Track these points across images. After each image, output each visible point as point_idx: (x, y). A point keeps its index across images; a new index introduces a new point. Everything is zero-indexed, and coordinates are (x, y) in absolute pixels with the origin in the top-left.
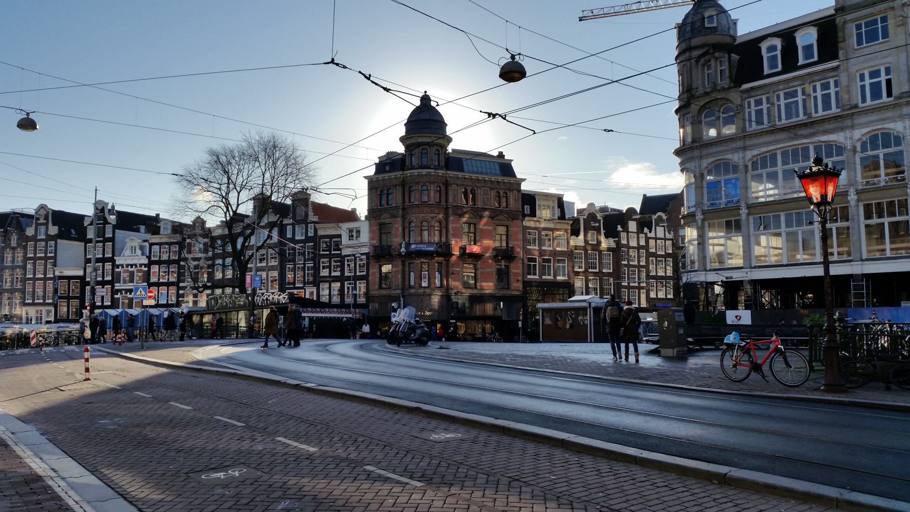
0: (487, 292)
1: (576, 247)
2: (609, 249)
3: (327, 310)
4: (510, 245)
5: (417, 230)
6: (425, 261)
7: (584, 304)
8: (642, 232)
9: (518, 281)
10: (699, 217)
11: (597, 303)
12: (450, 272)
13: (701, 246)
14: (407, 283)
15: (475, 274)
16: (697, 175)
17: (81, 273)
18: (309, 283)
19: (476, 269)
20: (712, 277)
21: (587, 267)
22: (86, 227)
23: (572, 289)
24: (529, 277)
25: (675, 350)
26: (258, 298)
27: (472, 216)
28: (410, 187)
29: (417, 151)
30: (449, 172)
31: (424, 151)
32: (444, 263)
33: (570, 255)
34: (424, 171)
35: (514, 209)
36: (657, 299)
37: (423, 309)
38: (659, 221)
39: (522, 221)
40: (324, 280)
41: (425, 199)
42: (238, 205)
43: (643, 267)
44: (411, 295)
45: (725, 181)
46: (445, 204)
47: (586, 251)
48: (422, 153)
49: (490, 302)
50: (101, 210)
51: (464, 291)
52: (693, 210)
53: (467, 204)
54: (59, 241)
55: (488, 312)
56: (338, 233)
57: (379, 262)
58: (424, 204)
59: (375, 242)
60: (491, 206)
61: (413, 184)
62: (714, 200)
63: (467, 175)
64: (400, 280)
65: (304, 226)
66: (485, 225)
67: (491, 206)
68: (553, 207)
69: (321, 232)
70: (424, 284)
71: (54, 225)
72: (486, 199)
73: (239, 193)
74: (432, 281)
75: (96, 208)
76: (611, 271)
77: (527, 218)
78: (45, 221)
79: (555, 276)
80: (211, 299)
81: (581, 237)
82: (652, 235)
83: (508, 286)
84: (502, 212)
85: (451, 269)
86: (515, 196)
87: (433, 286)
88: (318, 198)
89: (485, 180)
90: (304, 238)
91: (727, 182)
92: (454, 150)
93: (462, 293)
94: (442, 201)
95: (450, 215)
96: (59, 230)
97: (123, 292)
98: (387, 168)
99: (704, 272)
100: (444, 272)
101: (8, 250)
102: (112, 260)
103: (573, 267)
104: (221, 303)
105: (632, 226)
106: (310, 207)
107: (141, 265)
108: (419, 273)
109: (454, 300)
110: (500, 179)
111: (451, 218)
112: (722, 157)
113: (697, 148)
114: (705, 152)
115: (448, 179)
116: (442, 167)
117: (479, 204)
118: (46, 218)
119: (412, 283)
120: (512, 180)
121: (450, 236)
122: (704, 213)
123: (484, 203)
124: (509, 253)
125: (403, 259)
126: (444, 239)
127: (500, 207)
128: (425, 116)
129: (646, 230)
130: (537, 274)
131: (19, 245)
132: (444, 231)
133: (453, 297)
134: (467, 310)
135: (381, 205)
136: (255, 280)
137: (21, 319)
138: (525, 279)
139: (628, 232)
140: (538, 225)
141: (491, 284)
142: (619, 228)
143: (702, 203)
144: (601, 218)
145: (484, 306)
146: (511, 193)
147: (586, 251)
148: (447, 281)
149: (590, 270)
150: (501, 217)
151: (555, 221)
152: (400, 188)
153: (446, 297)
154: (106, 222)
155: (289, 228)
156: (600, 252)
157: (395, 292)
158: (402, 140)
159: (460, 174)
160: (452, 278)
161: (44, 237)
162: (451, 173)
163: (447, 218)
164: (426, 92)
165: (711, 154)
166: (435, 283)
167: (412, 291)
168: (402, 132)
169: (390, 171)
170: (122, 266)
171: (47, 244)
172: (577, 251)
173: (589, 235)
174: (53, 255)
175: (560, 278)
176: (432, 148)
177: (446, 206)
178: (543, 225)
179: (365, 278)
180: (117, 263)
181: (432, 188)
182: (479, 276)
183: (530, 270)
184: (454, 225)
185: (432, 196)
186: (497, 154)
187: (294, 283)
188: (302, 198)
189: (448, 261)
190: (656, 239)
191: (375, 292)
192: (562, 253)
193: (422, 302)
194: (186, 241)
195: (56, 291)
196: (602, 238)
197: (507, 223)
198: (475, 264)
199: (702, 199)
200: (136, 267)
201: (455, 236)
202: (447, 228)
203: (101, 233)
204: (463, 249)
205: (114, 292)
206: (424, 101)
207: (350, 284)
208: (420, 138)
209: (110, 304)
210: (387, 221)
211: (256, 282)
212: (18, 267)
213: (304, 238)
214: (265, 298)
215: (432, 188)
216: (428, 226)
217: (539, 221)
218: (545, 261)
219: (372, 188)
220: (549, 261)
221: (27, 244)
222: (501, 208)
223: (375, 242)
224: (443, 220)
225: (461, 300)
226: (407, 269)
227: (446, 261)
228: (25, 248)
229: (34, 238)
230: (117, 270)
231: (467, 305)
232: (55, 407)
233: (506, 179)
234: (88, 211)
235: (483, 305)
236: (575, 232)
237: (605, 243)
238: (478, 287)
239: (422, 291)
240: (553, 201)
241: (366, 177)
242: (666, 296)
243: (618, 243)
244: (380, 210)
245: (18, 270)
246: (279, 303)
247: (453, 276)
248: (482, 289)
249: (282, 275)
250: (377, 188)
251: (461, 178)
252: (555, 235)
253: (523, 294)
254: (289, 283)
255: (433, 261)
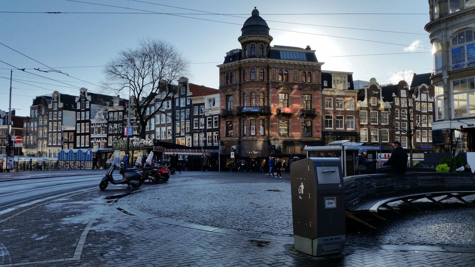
0: (296, 138)
1: (361, 108)
2: (386, 109)
3: (184, 150)
4: (313, 108)
5: (248, 98)
6: (253, 118)
7: (338, 147)
8: (411, 98)
9: (318, 131)
10: (445, 77)
11: (349, 146)
12: (270, 126)
13: (447, 100)
14: (242, 133)
15: (288, 127)
16: (444, 43)
17: (74, 129)
18: (188, 133)
19: (288, 123)
20: (456, 125)
21: (380, 122)
22: (76, 103)
23: (358, 137)
24: (326, 128)
25: (316, 242)
26: (138, 142)
27: (285, 88)
28: (244, 71)
29: (248, 47)
30: (269, 59)
31: (253, 46)
32: (266, 119)
33: (357, 113)
34: (252, 59)
35: (316, 84)
36: (422, 143)
37: (251, 150)
38: (423, 89)
39: (322, 91)
40: (195, 131)
41: (253, 78)
42: (143, 86)
43: (60, 121)
44: (244, 140)
45: (467, 46)
46: (266, 81)
47: (369, 111)
48: (251, 48)
49: (298, 145)
50: (84, 92)
51: (279, 138)
52: (440, 72)
53: (282, 81)
54: (64, 111)
55: (297, 152)
56: (203, 102)
57: (225, 120)
58: (253, 81)
59: (223, 107)
60: (299, 81)
61: (246, 68)
62: (458, 63)
63: (282, 61)
64: (238, 131)
65: (185, 98)
66: (294, 94)
67: (299, 81)
68: (344, 81)
69: (194, 102)
70: (253, 133)
71: (61, 102)
72: (295, 77)
73: (143, 79)
74: (257, 131)
75: (81, 92)
76: (388, 124)
77: (325, 89)
78: (57, 100)
79: (345, 128)
80: (114, 143)
81: (366, 101)
82: (418, 99)
83: (312, 134)
84: (307, 85)
85: (271, 124)
86: (317, 74)
87: (258, 135)
88: (191, 81)
89: (295, 64)
90: (185, 106)
91: (469, 47)
92: (275, 46)
93: (278, 139)
94: (265, 79)
95: (270, 88)
96: (64, 105)
97: (95, 139)
98: (231, 59)
99: (449, 121)
100: (266, 125)
101: (40, 116)
102: (89, 121)
103: (359, 122)
104: (119, 146)
105: (403, 93)
106: (188, 87)
107: (104, 124)
108: (249, 126)
109: (273, 144)
110: (306, 63)
111: (271, 90)
112: (465, 27)
113: (443, 22)
114: (450, 24)
115: (269, 64)
116: (265, 56)
117: (291, 81)
118: (58, 99)
119: (245, 133)
120: (314, 64)
121: (270, 101)
122: (449, 73)
123: (294, 80)
124: (312, 113)
125: (240, 118)
126: (266, 104)
127: (306, 82)
128: (254, 23)
129: (414, 96)
130: (333, 126)
131: (45, 113)
132: (266, 98)
133: (271, 142)
134: (282, 150)
135: (227, 84)
136: (129, 131)
137: (47, 154)
138: (324, 130)
139: (400, 97)
140: (333, 93)
141: (299, 133)
142: (394, 95)
143: (448, 66)
144: (381, 88)
145: (294, 148)
146: (314, 73)
147: (369, 111)
148: (268, 131)
149: (372, 124)
150: (306, 89)
151: (346, 91)
152: (238, 72)
153: (267, 142)
154: (86, 100)
155: (177, 101)
156: (380, 111)
157: (235, 139)
158: (240, 39)
159: (277, 61)
160: (271, 130)
161: (57, 109)
162: (271, 60)
163: (268, 90)
164: (255, 8)
165: (456, 25)
166: (259, 133)
167: (245, 138)
168: (240, 34)
169: (232, 61)
170: (94, 124)
171: (58, 113)
172: (362, 111)
173: (371, 100)
174: (61, 119)
175: (349, 129)
176: (258, 44)
177: (268, 82)
178: (336, 94)
179: (217, 130)
180: (92, 123)
181: (258, 71)
182: (290, 128)
183: (328, 124)
184: (273, 95)
185: (258, 75)
186: (306, 47)
187: (180, 134)
188: (184, 82)
189: (269, 118)
190: (421, 102)
191: (224, 139)
192: (350, 112)
193: (251, 145)
194: (126, 109)
195: (62, 138)
196: (381, 102)
197: (311, 92)
198: (288, 120)
199: (448, 62)
200: (101, 125)
201: (273, 102)
202: (268, 97)
203: (83, 105)
204: (279, 110)
205: (91, 139)
206: (254, 13)
207: (216, 133)
208: (250, 38)
209: (88, 146)
210: (231, 93)
211: (129, 132)
212: (45, 126)
213: (185, 106)
214: (141, 142)
215: (258, 71)
216: (255, 96)
217: (334, 91)
218: (338, 118)
219: (222, 73)
220: (341, 118)
221: (49, 113)
222: (307, 83)
223: (223, 107)
224: (266, 92)
225: (278, 144)
226: (242, 124)
227: (267, 118)
228: (48, 115)
229: (52, 110)
230: (92, 127)
231: (282, 147)
232: (256, 172)
233: (310, 63)
234: (77, 94)
235: (293, 147)
236: (361, 98)
237: (383, 105)
238: (290, 135)
239: (251, 138)
240: (345, 77)
241: (218, 66)
242: (428, 141)
243: (393, 106)
244: (226, 87)
245: (40, 128)
246: (148, 146)
247: (272, 128)
248: (293, 137)
249: (174, 129)
250: (225, 73)
251: (278, 63)
252: (345, 100)
253: (322, 140)
254: (177, 134)
255: (258, 118)
